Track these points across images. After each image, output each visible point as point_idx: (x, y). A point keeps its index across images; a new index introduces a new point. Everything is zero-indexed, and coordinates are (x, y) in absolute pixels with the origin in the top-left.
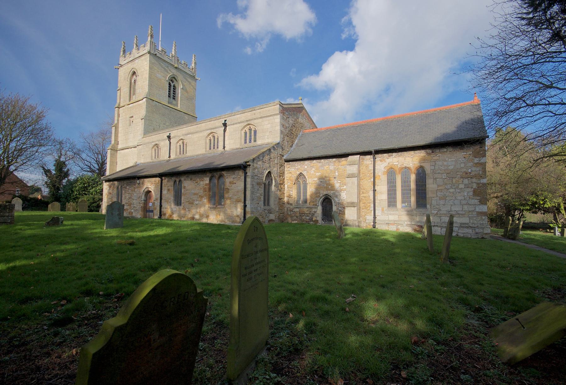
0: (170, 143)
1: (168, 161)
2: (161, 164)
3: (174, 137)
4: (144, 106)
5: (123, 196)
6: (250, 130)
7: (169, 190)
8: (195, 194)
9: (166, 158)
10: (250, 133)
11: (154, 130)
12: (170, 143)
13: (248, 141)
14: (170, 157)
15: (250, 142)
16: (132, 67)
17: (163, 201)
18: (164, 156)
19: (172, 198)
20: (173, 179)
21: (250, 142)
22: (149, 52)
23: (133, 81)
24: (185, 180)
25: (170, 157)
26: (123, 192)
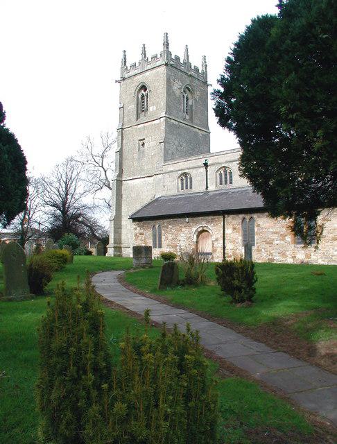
0: (207, 171)
1: (206, 193)
2: (189, 199)
3: (213, 164)
4: (163, 127)
5: (163, 237)
6: (225, 171)
7: (234, 229)
8: (274, 233)
9: (203, 189)
10: (226, 175)
11: (172, 159)
12: (207, 171)
13: (223, 182)
14: (207, 187)
15: (226, 183)
16: (141, 80)
17: (226, 241)
18: (198, 187)
19: (241, 238)
20: (241, 216)
21: (226, 183)
22: (166, 65)
23: (140, 96)
24: (259, 217)
25: (207, 187)
26: (163, 232)
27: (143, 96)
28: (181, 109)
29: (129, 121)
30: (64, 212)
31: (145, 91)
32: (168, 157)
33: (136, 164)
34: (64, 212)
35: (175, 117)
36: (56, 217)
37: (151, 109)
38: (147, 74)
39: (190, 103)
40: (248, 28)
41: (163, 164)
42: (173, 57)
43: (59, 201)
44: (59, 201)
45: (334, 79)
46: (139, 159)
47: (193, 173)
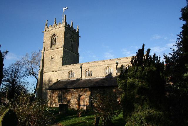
27: (54, 38)
28: (54, 51)
29: (47, 48)
30: (13, 85)
31: (54, 37)
32: (64, 64)
33: (49, 66)
34: (13, 85)
35: (58, 50)
36: (10, 87)
37: (57, 44)
38: (56, 30)
39: (72, 43)
40: (184, 25)
41: (62, 66)
42: (67, 24)
43: (11, 80)
44: (11, 80)
45: (86, 99)
46: (51, 64)
47: (74, 71)
